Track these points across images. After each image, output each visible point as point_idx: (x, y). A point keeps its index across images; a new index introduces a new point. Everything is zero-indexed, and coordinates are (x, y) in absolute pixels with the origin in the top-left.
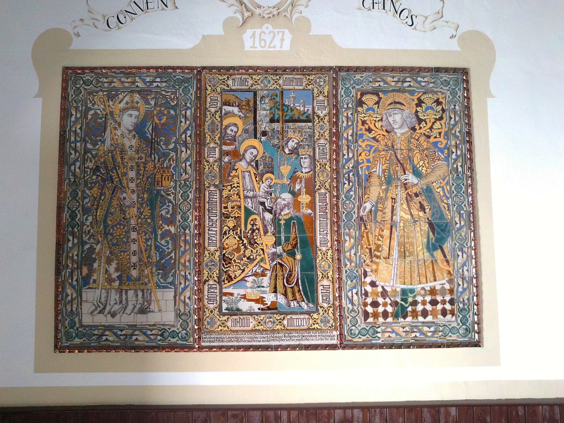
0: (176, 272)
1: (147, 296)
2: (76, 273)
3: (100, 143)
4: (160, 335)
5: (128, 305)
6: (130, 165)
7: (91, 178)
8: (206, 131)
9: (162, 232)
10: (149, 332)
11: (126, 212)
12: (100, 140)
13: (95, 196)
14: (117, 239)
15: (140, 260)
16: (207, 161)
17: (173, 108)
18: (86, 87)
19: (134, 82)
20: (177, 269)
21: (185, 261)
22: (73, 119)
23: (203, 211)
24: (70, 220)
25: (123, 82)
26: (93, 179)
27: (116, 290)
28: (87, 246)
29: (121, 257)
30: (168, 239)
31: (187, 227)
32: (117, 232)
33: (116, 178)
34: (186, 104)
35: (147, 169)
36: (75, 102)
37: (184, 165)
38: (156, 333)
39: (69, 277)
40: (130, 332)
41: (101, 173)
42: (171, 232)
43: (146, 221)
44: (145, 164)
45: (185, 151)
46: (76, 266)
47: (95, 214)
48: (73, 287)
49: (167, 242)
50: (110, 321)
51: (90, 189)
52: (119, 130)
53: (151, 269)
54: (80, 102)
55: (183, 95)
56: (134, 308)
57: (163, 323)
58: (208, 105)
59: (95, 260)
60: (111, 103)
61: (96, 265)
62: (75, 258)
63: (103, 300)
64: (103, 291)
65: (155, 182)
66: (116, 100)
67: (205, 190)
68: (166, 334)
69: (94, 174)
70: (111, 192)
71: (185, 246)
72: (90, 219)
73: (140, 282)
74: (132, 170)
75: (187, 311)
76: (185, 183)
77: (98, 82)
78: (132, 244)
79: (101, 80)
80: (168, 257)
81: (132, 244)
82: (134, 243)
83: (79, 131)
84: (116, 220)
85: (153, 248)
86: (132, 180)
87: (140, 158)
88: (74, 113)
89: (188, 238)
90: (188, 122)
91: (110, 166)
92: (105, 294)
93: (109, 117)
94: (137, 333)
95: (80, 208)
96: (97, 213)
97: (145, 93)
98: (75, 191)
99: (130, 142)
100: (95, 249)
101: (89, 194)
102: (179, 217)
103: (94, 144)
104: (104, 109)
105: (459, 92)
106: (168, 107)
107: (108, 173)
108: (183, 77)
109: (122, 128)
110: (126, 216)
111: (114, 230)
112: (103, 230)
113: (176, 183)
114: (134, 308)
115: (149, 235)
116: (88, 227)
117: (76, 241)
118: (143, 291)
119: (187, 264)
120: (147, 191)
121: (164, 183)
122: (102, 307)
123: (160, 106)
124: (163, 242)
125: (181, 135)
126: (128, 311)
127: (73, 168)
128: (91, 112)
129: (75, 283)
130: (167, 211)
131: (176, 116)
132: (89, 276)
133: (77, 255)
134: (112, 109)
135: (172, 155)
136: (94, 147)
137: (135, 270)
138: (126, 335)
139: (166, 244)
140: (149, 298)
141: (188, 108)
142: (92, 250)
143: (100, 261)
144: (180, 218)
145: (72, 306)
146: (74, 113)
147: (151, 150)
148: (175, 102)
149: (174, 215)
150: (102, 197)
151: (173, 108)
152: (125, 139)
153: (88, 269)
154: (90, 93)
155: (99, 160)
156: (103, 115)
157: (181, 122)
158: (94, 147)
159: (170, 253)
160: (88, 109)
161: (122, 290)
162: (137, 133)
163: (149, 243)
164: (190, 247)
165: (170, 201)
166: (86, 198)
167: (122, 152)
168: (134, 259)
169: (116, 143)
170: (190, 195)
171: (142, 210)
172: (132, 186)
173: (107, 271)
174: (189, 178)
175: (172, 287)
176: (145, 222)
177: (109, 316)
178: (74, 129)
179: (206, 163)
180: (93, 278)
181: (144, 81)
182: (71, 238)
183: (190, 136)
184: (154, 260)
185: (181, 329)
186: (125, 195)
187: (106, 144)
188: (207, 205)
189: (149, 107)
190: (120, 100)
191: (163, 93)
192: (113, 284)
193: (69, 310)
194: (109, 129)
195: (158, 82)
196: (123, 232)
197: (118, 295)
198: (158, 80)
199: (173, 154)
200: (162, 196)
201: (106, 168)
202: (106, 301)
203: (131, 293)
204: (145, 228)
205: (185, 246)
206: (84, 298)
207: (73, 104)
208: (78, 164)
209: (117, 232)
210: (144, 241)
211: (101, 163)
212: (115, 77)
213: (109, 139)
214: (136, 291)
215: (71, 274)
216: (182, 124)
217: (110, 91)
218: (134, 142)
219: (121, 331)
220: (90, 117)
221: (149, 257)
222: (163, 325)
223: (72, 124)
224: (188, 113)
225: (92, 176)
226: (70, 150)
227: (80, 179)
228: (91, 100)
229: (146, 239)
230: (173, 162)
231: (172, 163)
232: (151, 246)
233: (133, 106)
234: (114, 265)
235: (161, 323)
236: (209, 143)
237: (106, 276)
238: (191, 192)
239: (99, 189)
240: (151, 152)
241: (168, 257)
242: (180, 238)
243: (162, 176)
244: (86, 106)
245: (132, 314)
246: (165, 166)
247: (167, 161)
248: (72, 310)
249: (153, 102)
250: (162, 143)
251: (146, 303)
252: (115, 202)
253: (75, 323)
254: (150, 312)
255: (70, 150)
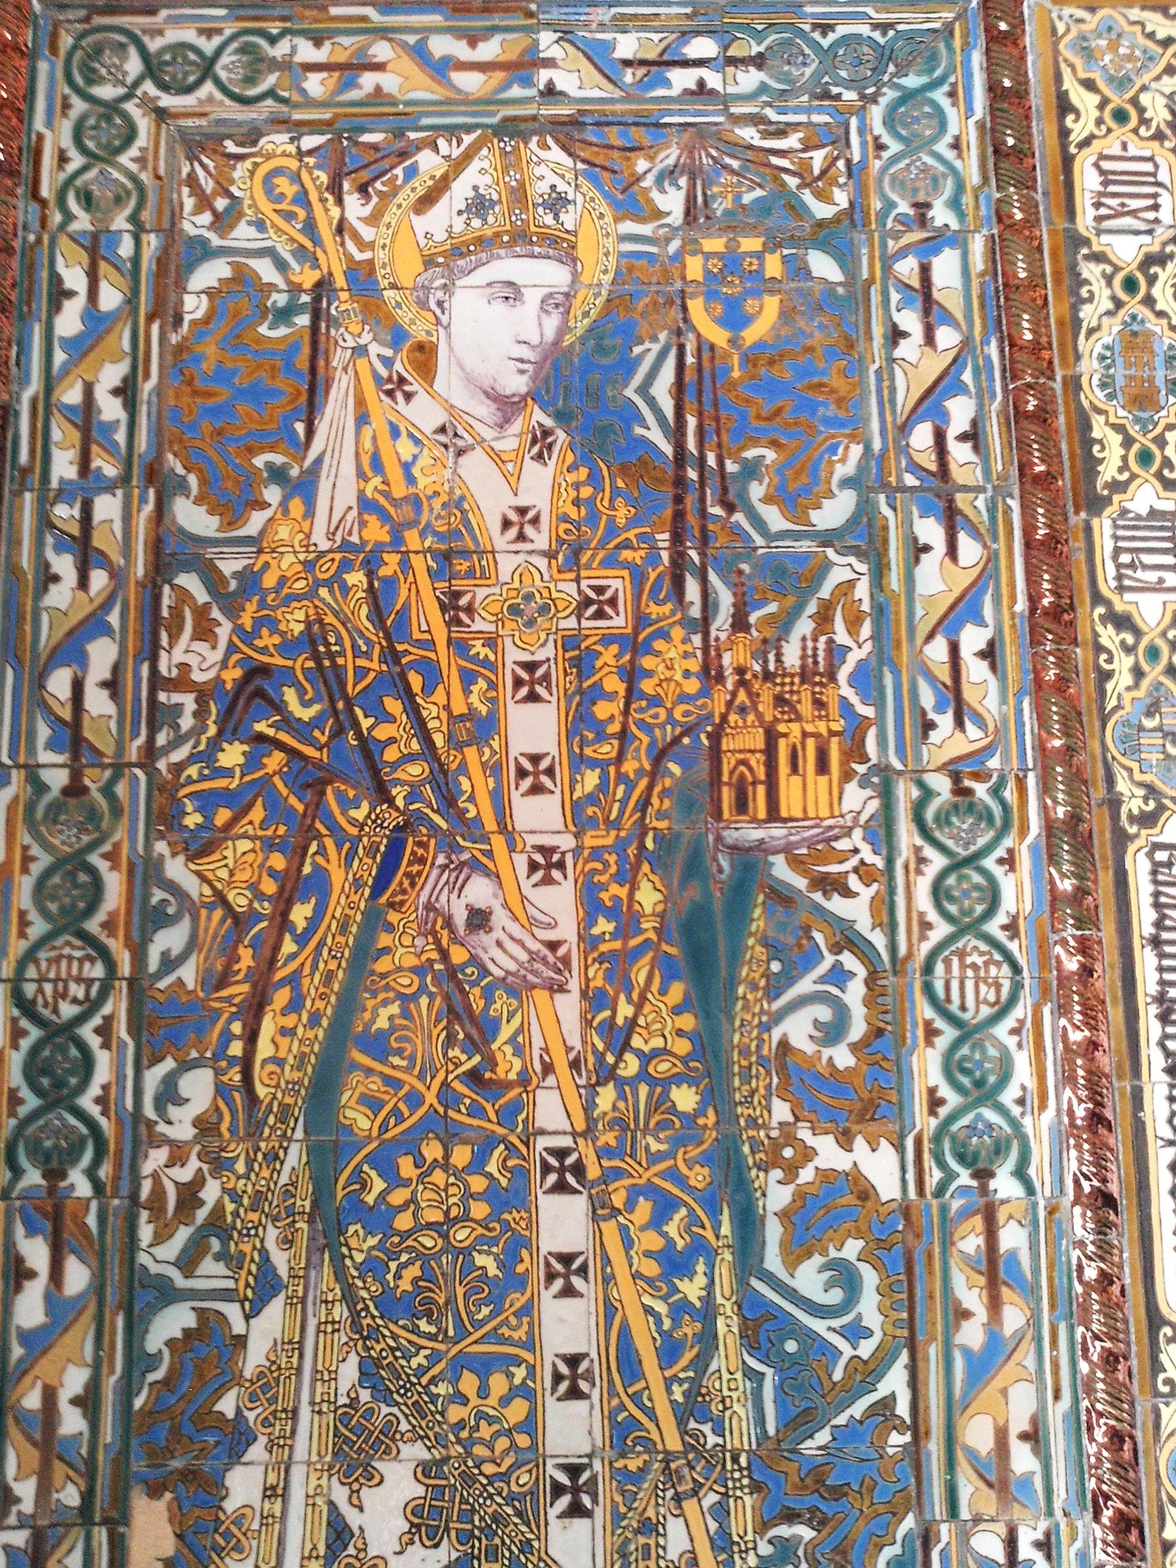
0: (927, 1538)
3: (272, 494)
6: (513, 655)
7: (207, 758)
8: (1093, 394)
9: (801, 1195)
11: (494, 1027)
12: (277, 474)
13: (239, 900)
14: (424, 1257)
15: (623, 1433)
16: (1123, 622)
17: (825, 235)
18: (167, 101)
19: (526, 64)
20: (939, 1509)
21: (1001, 1437)
22: (69, 322)
23: (1115, 1014)
24: (32, 1102)
25: (441, 68)
26: (228, 773)
28: (174, 1321)
29: (456, 1413)
30: (852, 1249)
31: (999, 1149)
32: (419, 1197)
33: (410, 758)
34: (922, 207)
35: (647, 686)
36: (87, 200)
37: (937, 651)
41: (288, 722)
42: (865, 1192)
43: (661, 1102)
44: (635, 644)
46: (71, 1496)
47: (236, 1049)
49: (844, 1277)
52: (421, 398)
53: (721, 1512)
54: (119, 201)
55: (895, 147)
58: (1086, 219)
59: (237, 1440)
60: (355, 208)
61: (243, 1486)
62: (72, 1422)
65: (715, 781)
66: (395, 191)
67: (1121, 839)
69: (230, 728)
70: (367, 868)
71: (995, 1306)
74: (533, 697)
77: (256, 64)
78: (547, 1295)
79: (280, 50)
80: (858, 1409)
81: (547, 1295)
82: (569, 1291)
83: (111, 409)
84: (414, 1099)
85: (727, 1326)
86: (535, 773)
87: (596, 604)
88: (74, 278)
89: (1012, 1237)
91: (362, 666)
93: (342, 304)
95: (117, 1006)
96: (251, 1038)
97: (614, 136)
98: (74, 864)
99: (512, 487)
100: (241, 1342)
102: (927, 1067)
103: (232, 502)
104: (301, 253)
105: (952, 114)
107: (344, 723)
108: (884, 27)
109: (446, 379)
110: (492, 1063)
111: (395, 1181)
112: (306, 1188)
113: (886, 794)
115: (693, 1220)
116: (177, 1157)
117: (77, 1277)
119: (1023, 1459)
120: (660, 863)
121: (790, 803)
123: (733, 224)
124: (809, 1279)
125: (905, 429)
127: (59, 684)
130: (824, 1013)
133: (88, 1402)
134: (362, 245)
135: (838, 576)
136: (231, 524)
137: (580, 1525)
139: (835, 1296)
141: (938, 240)
142: (210, 1349)
143: (281, 1444)
144: (935, 1077)
146: (74, 278)
147: (677, 538)
148: (842, 199)
149: (884, 1043)
150: (300, 914)
151: (825, 235)
153: (177, 1516)
154: (196, 145)
155: (272, 623)
156: (295, 289)
157: (896, 335)
159: (868, 1373)
162: (561, 417)
163: (692, 1289)
164: (1034, 1321)
165: (847, 939)
168: (571, 1429)
169: (399, 489)
171: (625, 1010)
172: (539, 816)
173: (340, 1533)
178: (72, 396)
179: (1108, 636)
181: (598, 58)
183: (973, 436)
184: (741, 1433)
186: (479, 891)
188: (1146, 962)
189: (646, 229)
190: (421, 184)
191: (749, 134)
196: (469, 1196)
199: (844, 568)
200: (782, 897)
201: (329, 679)
204: (655, 1158)
205: (995, 1306)
207: (69, 217)
208: (102, 655)
210: (651, 1268)
211: (288, 647)
212: (383, 33)
213: (348, 468)
216: (907, 350)
217: (342, 128)
218: (539, 485)
220: (194, 306)
221: (694, 1406)
223: (59, 357)
224: (946, 269)
225: (215, 745)
226: (39, 544)
227: (119, 769)
228: (209, 185)
230: (853, 625)
231: (842, 637)
232: (708, 1312)
233: (526, 230)
234: (399, 1484)
236: (1117, 487)
238: (1009, 861)
240: (679, 563)
241: (858, 1409)
242: (948, 1242)
243: (772, 737)
244: (170, 231)
246: (792, 656)
247: (804, 626)
249: (672, 202)
250: (756, 491)
252: (403, 951)
255: (39, 544)
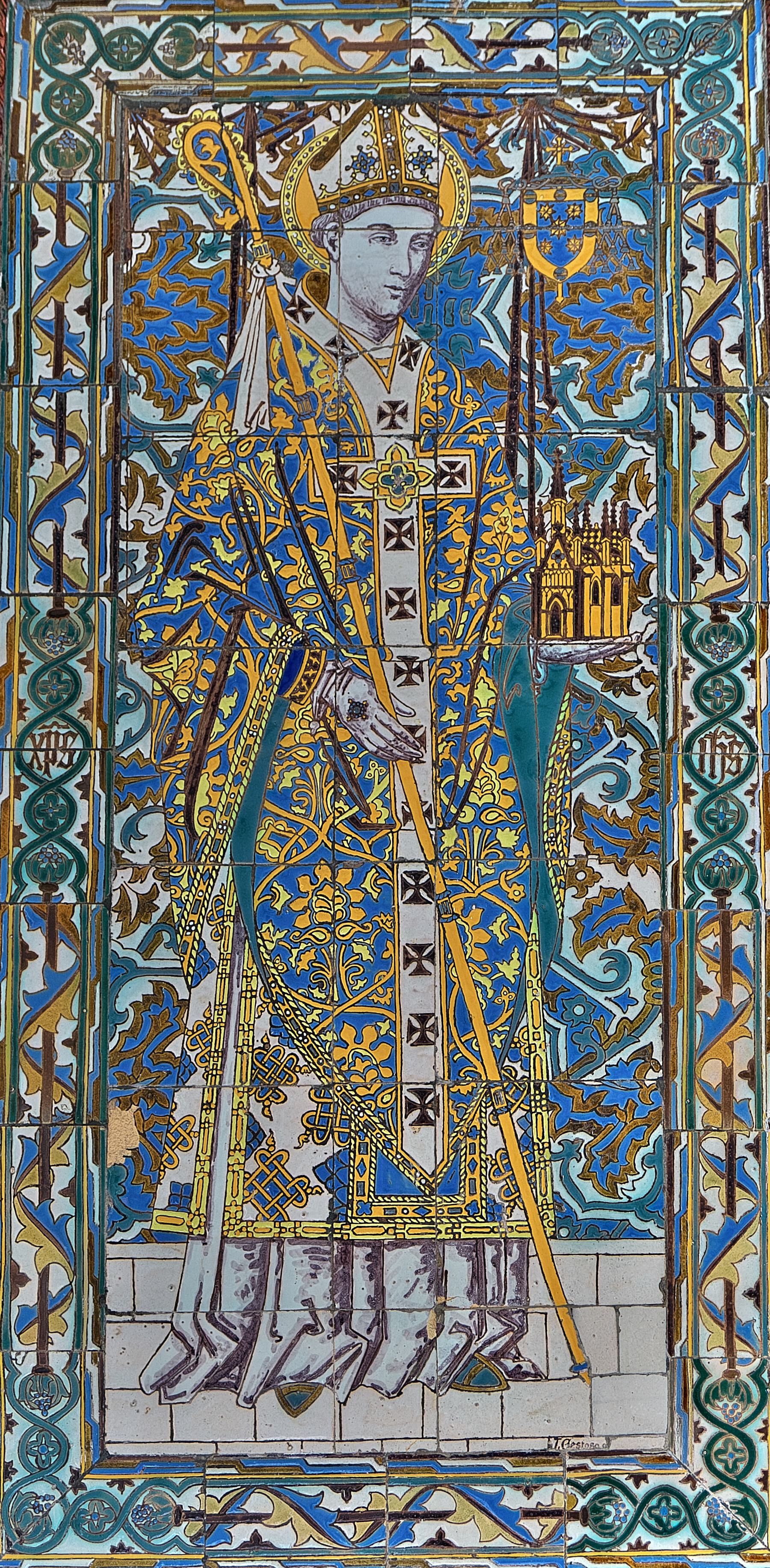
0: (671, 1141)
1: (502, 1284)
2: (70, 1148)
3: (203, 392)
4: (583, 1517)
5: (383, 1335)
6: (386, 514)
9: (587, 905)
10: (514, 1500)
11: (369, 785)
12: (207, 377)
13: (182, 695)
15: (456, 1068)
17: (632, 187)
18: (116, 75)
20: (681, 1123)
22: (43, 254)
24: (31, 836)
26: (172, 601)
27: (314, 1248)
28: (137, 990)
29: (338, 1053)
30: (625, 943)
31: (735, 875)
33: (306, 591)
37: (705, 514)
38: (560, 1503)
39: (23, 1173)
40: (400, 1496)
41: (216, 564)
42: (636, 904)
43: (489, 841)
44: (477, 507)
45: (711, 435)
46: (65, 1105)
47: (180, 800)
48: (53, 1230)
50: (277, 1431)
51: (152, 655)
52: (318, 317)
53: (526, 1123)
54: (80, 157)
55: (691, 114)
56: (422, 1356)
57: (600, 1443)
59: (182, 1070)
60: (265, 164)
61: (187, 1102)
62: (65, 1057)
63: (232, 1305)
64: (235, 1254)
66: (297, 149)
68: (621, 1510)
69: (174, 567)
70: (276, 672)
71: (726, 985)
72: (153, 827)
73: (464, 1199)
74: (400, 546)
75: (745, 1372)
76: (718, 618)
77: (186, 45)
78: (405, 973)
80: (625, 1055)
81: (405, 973)
82: (420, 971)
83: (77, 324)
84: (311, 837)
85: (534, 996)
86: (401, 603)
88: (47, 219)
90: (725, 270)
91: (271, 521)
92: (248, 1274)
93: (256, 242)
94: (439, 1501)
95: (92, 768)
96: (192, 792)
97: (469, 105)
98: (58, 666)
100: (185, 1004)
101: (146, 683)
102: (685, 817)
103: (174, 399)
106: (609, 183)
110: (367, 812)
114: (422, 1356)
116: (139, 874)
117: (66, 958)
118: (474, 1251)
120: (493, 671)
121: (591, 615)
122: (226, 1347)
123: (560, 181)
124: (593, 964)
125: (687, 343)
126: (384, 1372)
127: (44, 534)
128: (153, 217)
129: (61, 1206)
130: (611, 779)
131: (655, 232)
132: (148, 1160)
133: (75, 1043)
136: (171, 414)
137: (426, 1131)
138: (374, 1516)
139: (612, 976)
140: (511, 1295)
141: (724, 189)
142: (163, 1007)
143: (215, 1075)
145: (43, 1341)
146: (47, 219)
147: (511, 426)
148: (647, 157)
149: (655, 799)
150: (226, 704)
152: (358, 371)
154: (139, 111)
155: (205, 492)
156: (219, 230)
157: (685, 268)
158: (171, 414)
160: (128, 203)
161: (348, 1245)
163: (509, 970)
165: (629, 725)
166: (124, 707)
167: (336, 439)
168: (420, 1065)
169: (301, 389)
170: (749, 686)
171: (465, 776)
172: (404, 635)
173: (255, 1134)
174: (739, 588)
175: (651, 1226)
176: (485, 843)
177: (269, 1401)
180: (170, 1176)
181: (458, 40)
182: (37, 941)
183: (741, 349)
185: (708, 1480)
186: (358, 689)
187: (242, 401)
189: (493, 183)
190: (317, 145)
191: (575, 103)
192: (293, 1212)
193: (27, 1365)
194: (256, 306)
195: (539, 44)
197: (324, 1281)
198: (541, 31)
199: (637, 450)
200: (585, 696)
201: (247, 532)
202: (254, 1311)
203: (402, 1264)
204: (484, 879)
205: (726, 985)
206: (117, 1298)
207: (41, 170)
208: (76, 513)
209: (319, 903)
210: (480, 955)
213: (261, 372)
214: (432, 1251)
215: (40, 1158)
217: (254, 100)
219: (347, 1490)
220: (140, 244)
222: (596, 1454)
223: (36, 282)
224: (727, 215)
225: (162, 580)
226: (26, 428)
227: (91, 597)
228: (150, 146)
229: (367, 903)
230: (642, 495)
231: (634, 502)
232: (520, 986)
233: (392, 182)
234: (299, 1100)
235: (587, 1443)
237: (252, 1165)
238: (752, 670)
239: (203, 654)
240: (512, 443)
242: (694, 940)
243: (579, 577)
244: (121, 183)
245: (413, 1391)
246: (596, 519)
247: (606, 494)
248: (42, 1369)
249: (513, 159)
250: (573, 390)
251: (494, 1327)
252: (301, 730)
253: (63, 1448)
254: (518, 1375)
255: (26, 428)
